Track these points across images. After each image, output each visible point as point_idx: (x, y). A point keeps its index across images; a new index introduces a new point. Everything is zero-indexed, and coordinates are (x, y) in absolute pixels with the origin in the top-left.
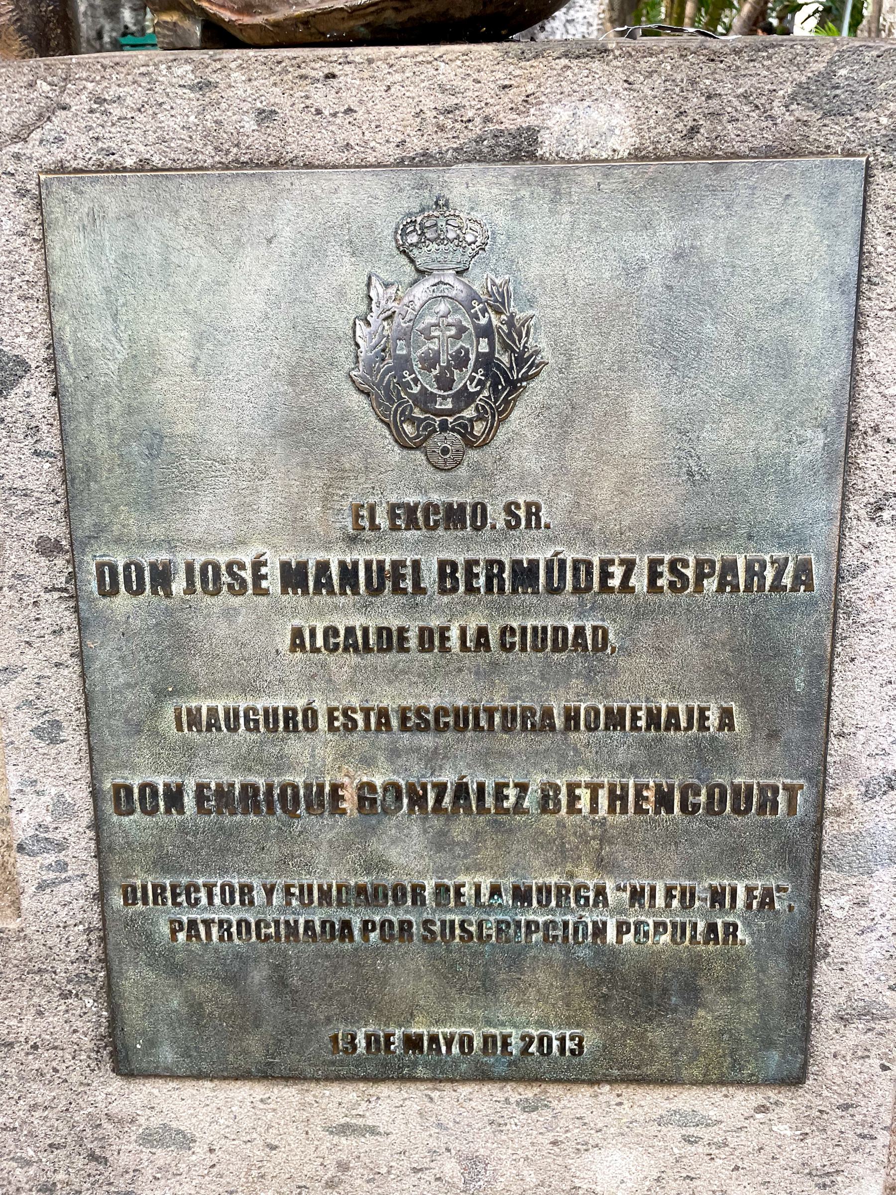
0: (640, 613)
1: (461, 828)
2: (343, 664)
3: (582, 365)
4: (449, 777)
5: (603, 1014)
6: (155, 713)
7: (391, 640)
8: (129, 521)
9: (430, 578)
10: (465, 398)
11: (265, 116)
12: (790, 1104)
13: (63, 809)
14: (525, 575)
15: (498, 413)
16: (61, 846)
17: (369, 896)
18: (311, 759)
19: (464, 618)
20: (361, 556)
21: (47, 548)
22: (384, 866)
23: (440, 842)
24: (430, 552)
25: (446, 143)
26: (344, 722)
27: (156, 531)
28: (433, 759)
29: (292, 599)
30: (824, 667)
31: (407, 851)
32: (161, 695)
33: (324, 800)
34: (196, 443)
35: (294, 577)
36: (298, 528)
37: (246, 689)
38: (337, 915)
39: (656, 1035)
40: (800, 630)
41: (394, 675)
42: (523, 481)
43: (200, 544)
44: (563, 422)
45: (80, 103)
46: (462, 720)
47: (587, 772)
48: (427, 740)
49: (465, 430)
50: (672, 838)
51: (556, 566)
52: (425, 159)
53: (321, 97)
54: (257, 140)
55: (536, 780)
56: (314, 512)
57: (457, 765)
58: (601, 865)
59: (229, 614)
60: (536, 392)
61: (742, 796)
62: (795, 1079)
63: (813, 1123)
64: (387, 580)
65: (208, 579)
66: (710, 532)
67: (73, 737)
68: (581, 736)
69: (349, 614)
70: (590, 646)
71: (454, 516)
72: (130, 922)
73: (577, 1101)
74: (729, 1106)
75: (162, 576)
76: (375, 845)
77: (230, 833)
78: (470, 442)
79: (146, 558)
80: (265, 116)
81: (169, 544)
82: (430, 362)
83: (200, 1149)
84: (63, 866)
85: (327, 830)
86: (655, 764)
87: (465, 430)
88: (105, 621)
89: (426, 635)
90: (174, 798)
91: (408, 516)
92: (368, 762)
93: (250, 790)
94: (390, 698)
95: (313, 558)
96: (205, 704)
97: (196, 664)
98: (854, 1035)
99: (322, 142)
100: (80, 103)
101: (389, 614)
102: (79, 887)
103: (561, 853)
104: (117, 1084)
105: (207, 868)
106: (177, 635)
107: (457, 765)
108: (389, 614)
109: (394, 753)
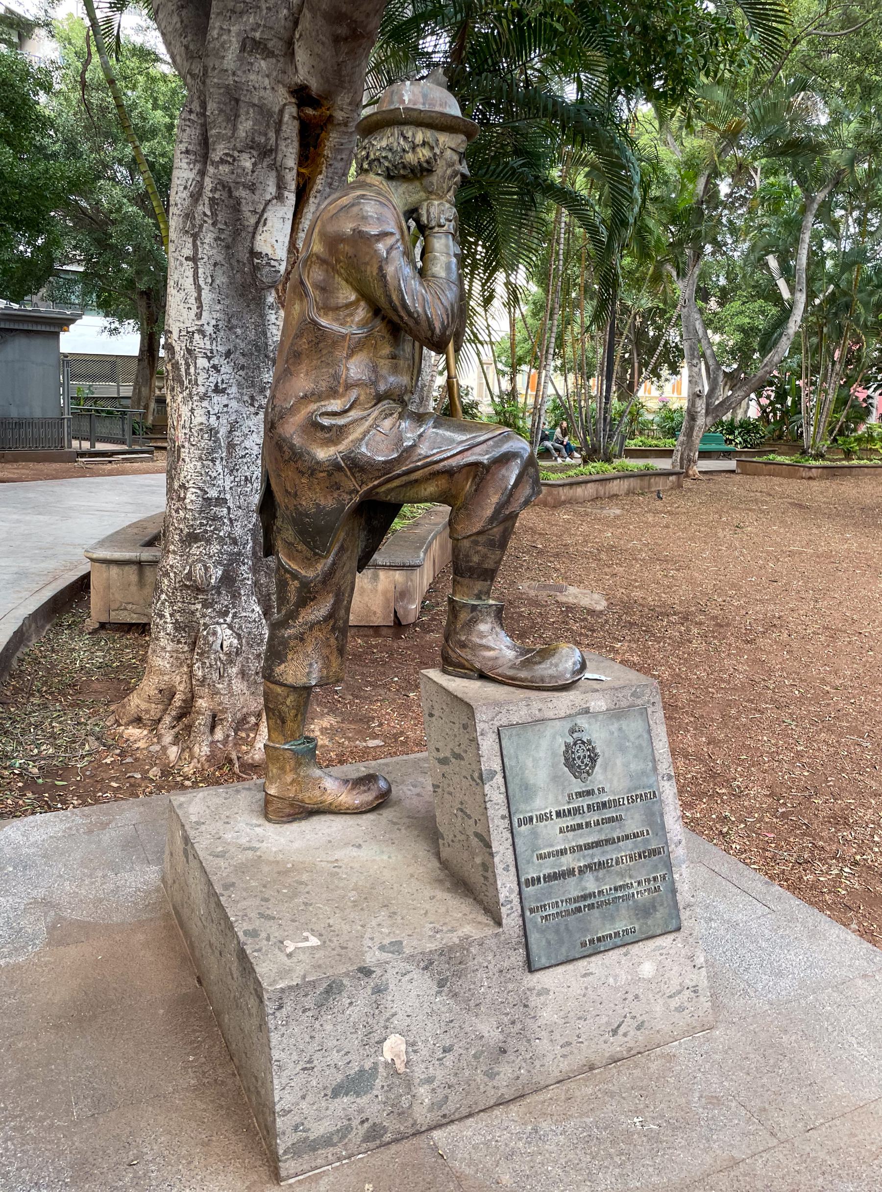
0: (627, 810)
1: (601, 873)
2: (570, 835)
3: (606, 755)
4: (596, 860)
5: (638, 919)
6: (532, 857)
7: (580, 826)
8: (522, 806)
9: (586, 809)
10: (587, 765)
11: (540, 710)
12: (679, 936)
13: (511, 891)
14: (604, 804)
15: (593, 767)
16: (511, 902)
17: (584, 897)
18: (568, 861)
19: (594, 817)
20: (571, 806)
21: (503, 817)
22: (586, 889)
23: (597, 879)
24: (584, 802)
25: (573, 712)
26: (573, 850)
27: (528, 808)
28: (592, 856)
29: (559, 820)
30: (662, 815)
31: (590, 884)
32: (533, 851)
33: (570, 872)
34: (534, 785)
35: (558, 814)
36: (557, 802)
37: (552, 846)
38: (577, 905)
39: (649, 922)
40: (656, 808)
41: (581, 836)
42: (600, 783)
43: (538, 810)
44: (605, 768)
45: (504, 711)
46: (598, 844)
47: (627, 848)
48: (590, 851)
49: (588, 772)
50: (643, 866)
51: (609, 801)
52: (570, 716)
53: (550, 705)
54: (539, 715)
55: (614, 857)
56: (560, 797)
57: (598, 855)
58: (631, 877)
59: (546, 826)
60: (599, 762)
61: (654, 850)
62: (678, 929)
63: (685, 941)
64: (577, 811)
65: (541, 818)
66: (636, 789)
67: (513, 869)
68: (621, 843)
69: (570, 821)
70: (619, 819)
71: (589, 793)
72: (531, 920)
73: (635, 949)
74: (665, 941)
75: (531, 819)
76: (583, 883)
77: (551, 887)
78: (589, 775)
79: (527, 815)
80: (540, 710)
81: (531, 811)
82: (579, 758)
83: (551, 993)
84: (512, 908)
85: (572, 881)
86: (636, 847)
87: (588, 772)
88: (519, 833)
89: (587, 823)
90: (539, 879)
91: (580, 794)
92: (579, 860)
93: (555, 873)
94: (581, 842)
95: (561, 808)
96: (542, 852)
97: (540, 841)
98: (688, 913)
99: (550, 714)
100: (504, 711)
101: (578, 820)
102: (516, 914)
103: (622, 875)
104: (529, 976)
105: (547, 899)
106: (535, 834)
107: (598, 855)
108: (578, 820)
109: (584, 857)
